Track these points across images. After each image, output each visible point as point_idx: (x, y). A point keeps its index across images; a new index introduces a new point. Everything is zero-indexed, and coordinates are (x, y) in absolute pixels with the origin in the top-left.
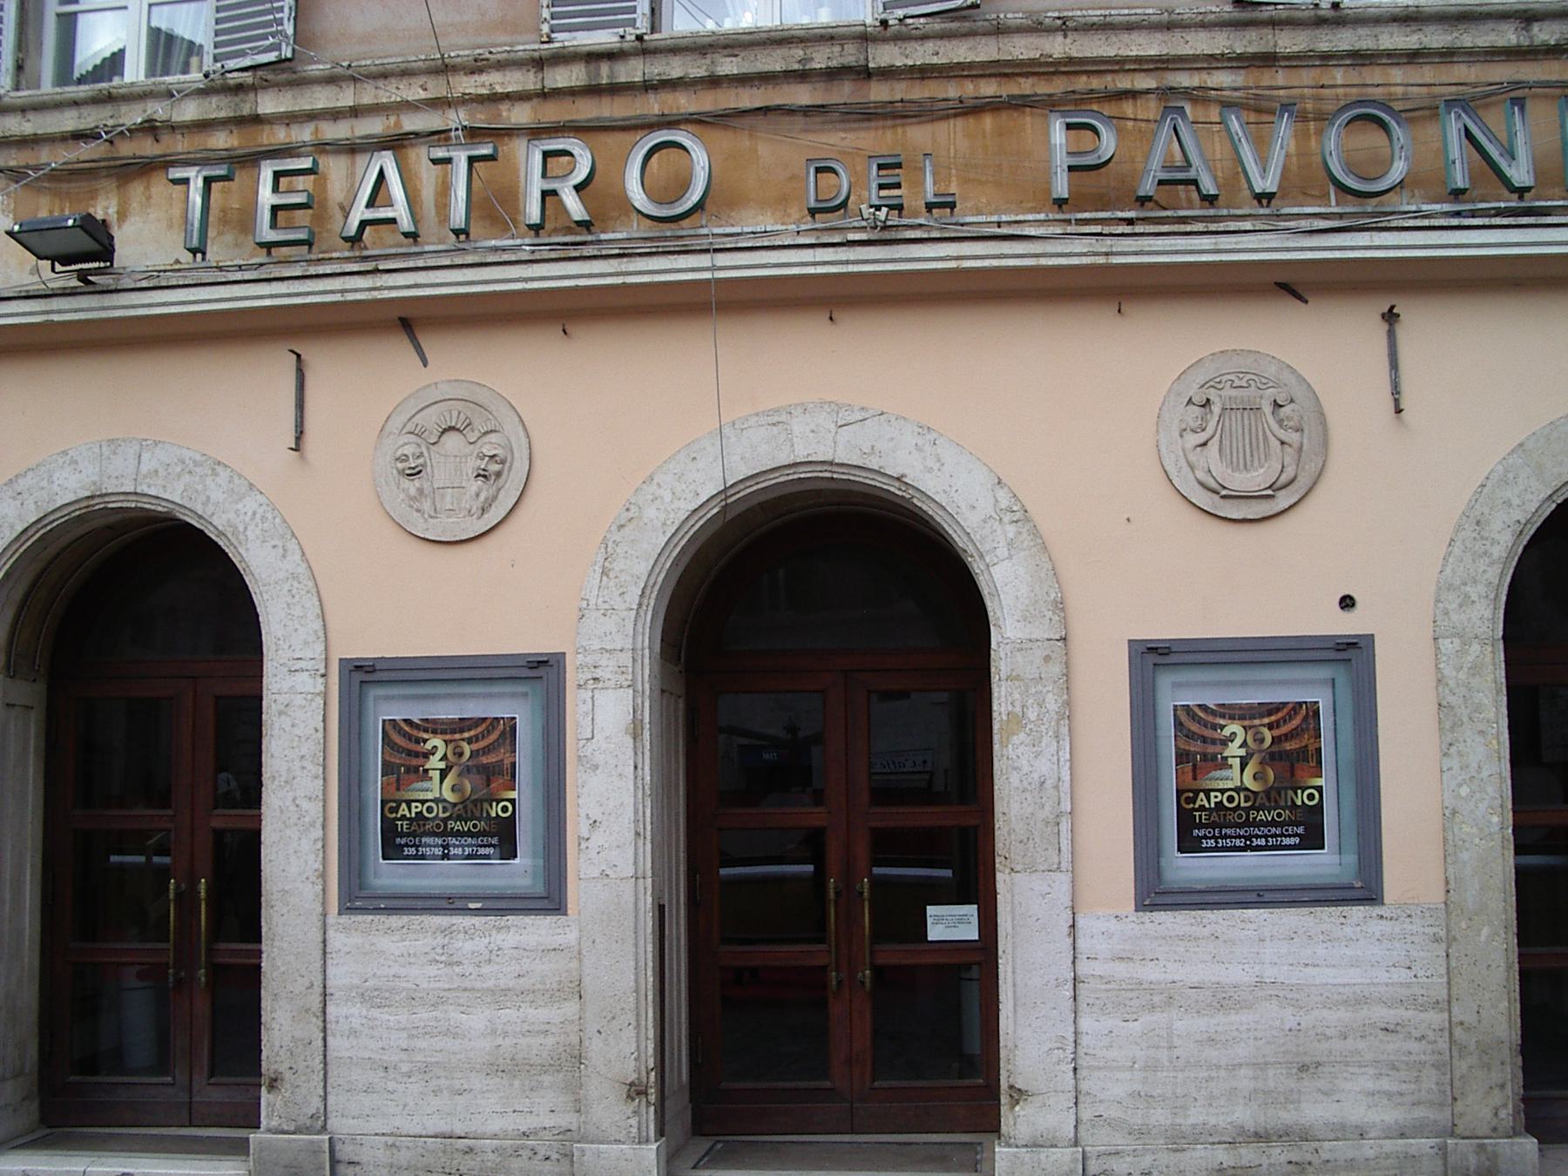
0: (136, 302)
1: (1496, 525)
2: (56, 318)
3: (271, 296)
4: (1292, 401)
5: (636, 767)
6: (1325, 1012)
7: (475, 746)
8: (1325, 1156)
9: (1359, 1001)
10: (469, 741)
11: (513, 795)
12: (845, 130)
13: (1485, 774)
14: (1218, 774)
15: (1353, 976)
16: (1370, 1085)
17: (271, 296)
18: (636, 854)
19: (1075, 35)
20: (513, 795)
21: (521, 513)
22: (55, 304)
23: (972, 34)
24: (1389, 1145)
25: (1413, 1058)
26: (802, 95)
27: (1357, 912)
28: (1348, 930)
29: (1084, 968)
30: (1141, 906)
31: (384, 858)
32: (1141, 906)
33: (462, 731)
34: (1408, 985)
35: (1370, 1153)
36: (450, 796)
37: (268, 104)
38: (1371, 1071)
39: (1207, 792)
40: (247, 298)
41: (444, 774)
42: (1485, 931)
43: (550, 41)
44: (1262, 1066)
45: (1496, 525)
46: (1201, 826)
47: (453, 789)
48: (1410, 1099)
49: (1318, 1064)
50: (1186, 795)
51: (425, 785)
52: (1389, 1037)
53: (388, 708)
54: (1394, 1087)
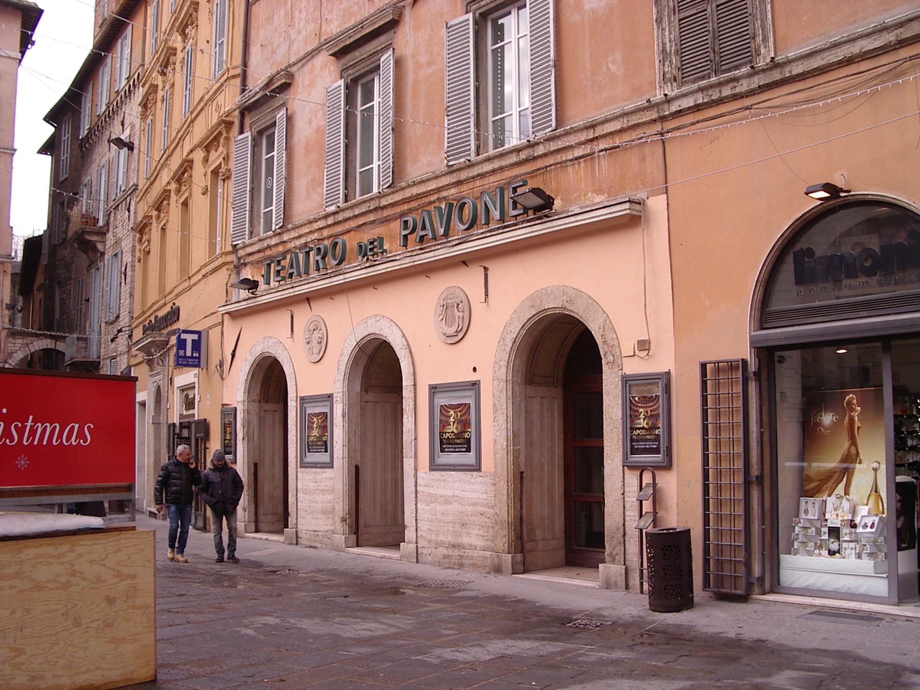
0: (556, 225)
1: (508, 340)
2: (249, 305)
3: (279, 296)
4: (462, 302)
5: (343, 426)
6: (468, 507)
7: (461, 413)
8: (467, 554)
9: (475, 504)
10: (321, 419)
11: (470, 430)
12: (379, 227)
13: (503, 427)
14: (448, 427)
15: (474, 495)
16: (478, 532)
17: (279, 296)
18: (343, 451)
19: (418, 186)
20: (470, 430)
21: (327, 352)
22: (249, 301)
23: (397, 191)
24: (481, 553)
25: (487, 524)
26: (371, 217)
27: (475, 473)
28: (473, 479)
29: (419, 488)
30: (431, 470)
31: (441, 452)
32: (431, 470)
33: (458, 408)
34: (486, 500)
35: (476, 555)
36: (455, 431)
37: (285, 237)
38: (478, 527)
39: (446, 433)
40: (354, 277)
41: (644, 419)
42: (502, 483)
43: (325, 210)
44: (454, 523)
45: (508, 340)
46: (445, 444)
47: (456, 428)
48: (486, 538)
49: (466, 524)
50: (441, 434)
51: (449, 427)
52: (482, 517)
53: (442, 400)
54: (483, 534)
